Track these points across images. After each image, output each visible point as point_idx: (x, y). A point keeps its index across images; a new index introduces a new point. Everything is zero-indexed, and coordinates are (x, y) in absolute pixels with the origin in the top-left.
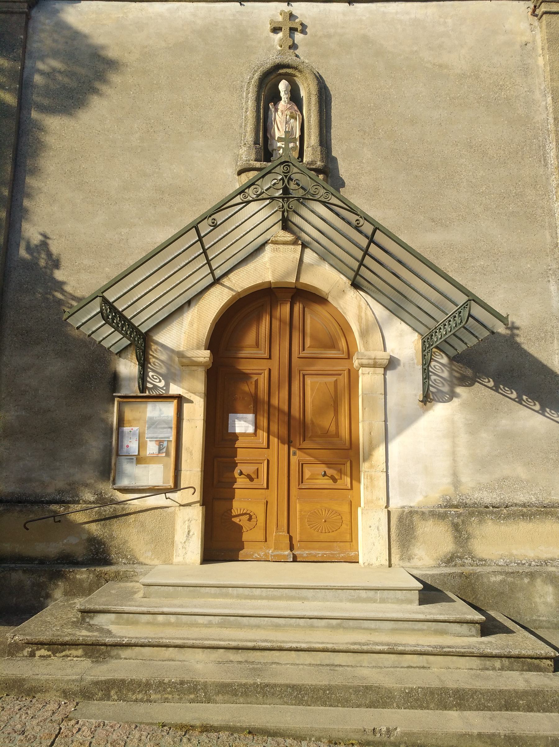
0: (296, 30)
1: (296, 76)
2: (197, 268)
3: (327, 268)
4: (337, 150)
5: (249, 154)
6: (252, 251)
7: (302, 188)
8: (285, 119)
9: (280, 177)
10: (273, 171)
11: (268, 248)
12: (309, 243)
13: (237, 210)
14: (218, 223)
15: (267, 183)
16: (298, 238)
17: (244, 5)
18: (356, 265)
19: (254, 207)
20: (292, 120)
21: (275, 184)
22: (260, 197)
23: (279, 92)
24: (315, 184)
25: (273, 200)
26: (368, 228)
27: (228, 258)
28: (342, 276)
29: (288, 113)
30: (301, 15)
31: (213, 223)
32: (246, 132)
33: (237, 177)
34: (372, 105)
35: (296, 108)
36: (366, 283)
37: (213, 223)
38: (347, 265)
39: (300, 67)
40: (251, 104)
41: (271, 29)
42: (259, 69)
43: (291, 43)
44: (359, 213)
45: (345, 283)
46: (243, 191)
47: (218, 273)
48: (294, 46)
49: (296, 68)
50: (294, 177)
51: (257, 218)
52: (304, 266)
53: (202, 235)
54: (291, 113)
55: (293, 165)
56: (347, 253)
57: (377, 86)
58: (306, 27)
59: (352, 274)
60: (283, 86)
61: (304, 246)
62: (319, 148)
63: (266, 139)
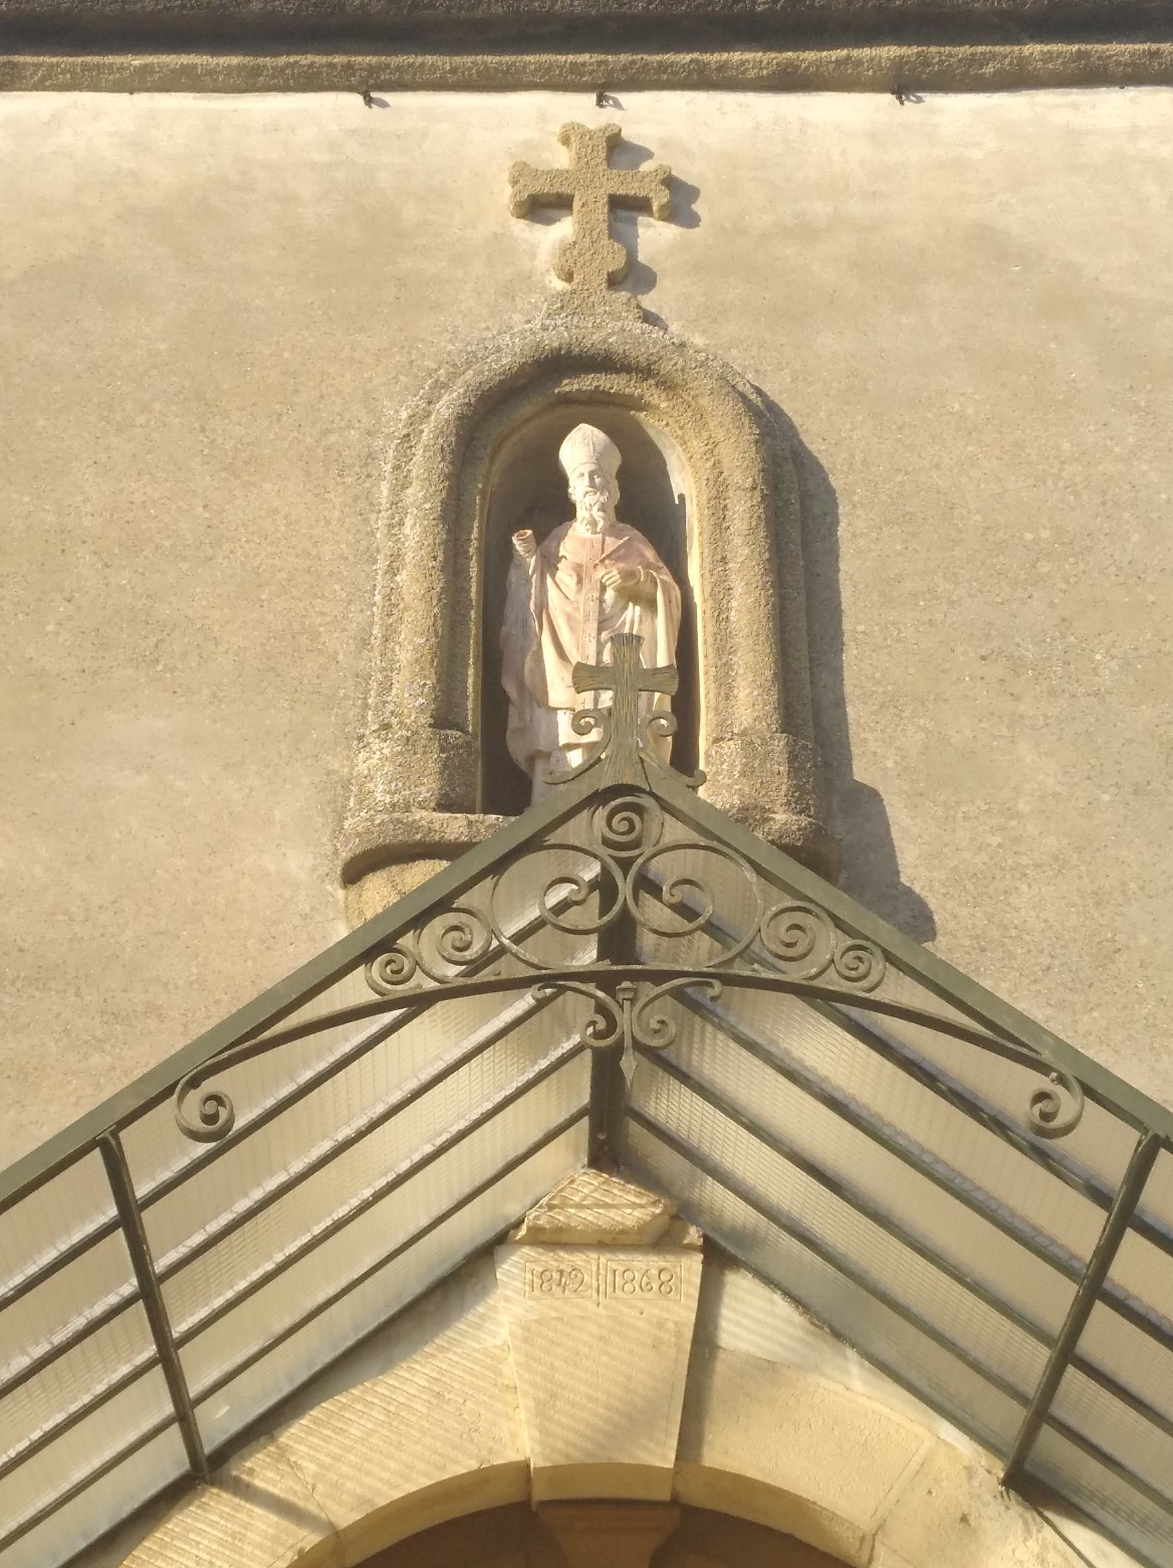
0: (641, 205)
1: (639, 404)
2: (100, 1389)
3: (858, 1386)
4: (876, 756)
5: (404, 772)
6: (418, 1289)
7: (711, 928)
8: (593, 606)
9: (590, 872)
10: (553, 838)
11: (515, 1269)
12: (746, 1238)
13: (347, 1048)
14: (240, 1123)
15: (516, 908)
16: (683, 1212)
17: (384, 105)
18: (1031, 1360)
19: (429, 1040)
20: (633, 612)
21: (562, 907)
22: (486, 975)
23: (561, 481)
24: (789, 902)
25: (562, 990)
26: (1105, 1145)
27: (279, 1327)
28: (948, 1432)
29: (612, 575)
30: (664, 144)
31: (210, 1119)
32: (390, 668)
33: (341, 893)
34: (1045, 534)
35: (650, 554)
36: (1092, 1472)
37: (210, 1119)
38: (976, 1366)
39: (665, 367)
40: (417, 534)
41: (519, 205)
42: (454, 376)
43: (616, 261)
44: (1046, 1056)
45: (970, 1471)
46: (386, 945)
47: (219, 1420)
48: (632, 277)
49: (646, 372)
50: (666, 868)
51: (447, 1100)
52: (721, 1370)
53: (141, 1190)
54: (628, 575)
55: (666, 807)
56: (977, 1288)
57: (1066, 446)
58: (693, 193)
59: (1010, 1418)
60: (580, 452)
61: (719, 1257)
62: (779, 744)
63: (495, 704)
